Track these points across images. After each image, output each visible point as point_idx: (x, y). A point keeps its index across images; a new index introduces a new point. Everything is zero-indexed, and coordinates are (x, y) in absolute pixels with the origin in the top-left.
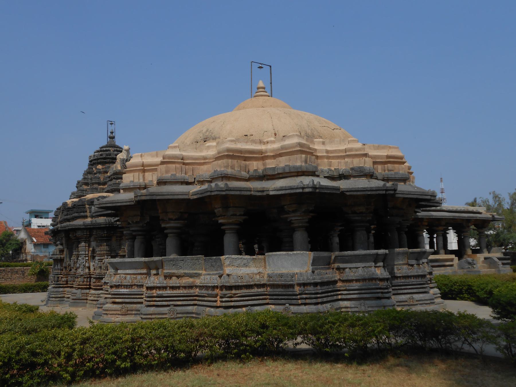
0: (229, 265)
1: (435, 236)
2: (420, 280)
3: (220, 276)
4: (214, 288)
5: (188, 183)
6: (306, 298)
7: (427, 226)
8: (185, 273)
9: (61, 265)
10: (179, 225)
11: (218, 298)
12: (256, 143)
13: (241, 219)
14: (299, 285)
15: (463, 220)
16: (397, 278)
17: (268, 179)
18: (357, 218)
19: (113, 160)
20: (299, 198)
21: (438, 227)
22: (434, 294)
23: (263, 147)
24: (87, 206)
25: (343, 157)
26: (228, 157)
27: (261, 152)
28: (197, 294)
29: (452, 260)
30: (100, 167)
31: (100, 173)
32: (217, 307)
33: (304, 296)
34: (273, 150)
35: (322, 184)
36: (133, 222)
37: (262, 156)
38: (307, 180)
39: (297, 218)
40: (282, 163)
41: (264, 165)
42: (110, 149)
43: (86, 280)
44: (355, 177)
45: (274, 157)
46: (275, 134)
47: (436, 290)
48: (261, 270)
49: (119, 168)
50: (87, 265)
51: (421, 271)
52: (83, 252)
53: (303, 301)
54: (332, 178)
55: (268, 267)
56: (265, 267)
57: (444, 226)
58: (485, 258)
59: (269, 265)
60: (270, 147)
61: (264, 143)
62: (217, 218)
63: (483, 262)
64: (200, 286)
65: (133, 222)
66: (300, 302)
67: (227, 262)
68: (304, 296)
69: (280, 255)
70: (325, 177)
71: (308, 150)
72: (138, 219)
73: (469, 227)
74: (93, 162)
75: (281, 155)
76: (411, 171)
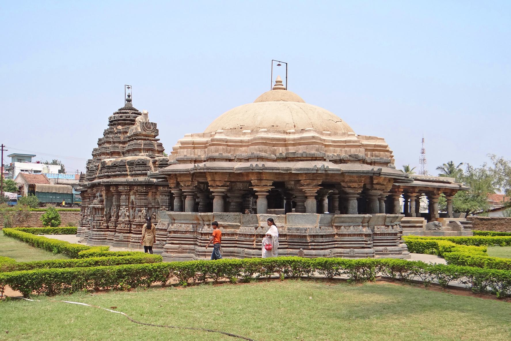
0: (262, 220)
1: (409, 200)
2: (393, 237)
3: (256, 228)
4: (251, 235)
5: (230, 160)
6: (315, 245)
7: (403, 192)
8: (229, 225)
9: (102, 214)
10: (223, 190)
11: (254, 243)
12: (281, 133)
13: (269, 188)
14: (311, 236)
15: (434, 188)
16: (376, 234)
17: (289, 161)
18: (351, 191)
19: (132, 122)
20: (312, 175)
21: (411, 192)
22: (402, 248)
23: (286, 137)
24: (127, 166)
25: (344, 147)
26: (263, 144)
27: (285, 140)
28: (237, 239)
29: (422, 222)
30: (120, 127)
31: (120, 133)
32: (254, 249)
33: (314, 244)
34: (294, 140)
35: (330, 167)
36: (185, 185)
37: (285, 143)
38: (319, 164)
39: (311, 190)
40: (301, 150)
41: (287, 150)
42: (129, 111)
43: (127, 226)
44: (351, 161)
45: (294, 145)
46: (295, 126)
47: (404, 245)
48: (283, 224)
49: (140, 130)
50: (127, 214)
51: (393, 230)
52: (124, 204)
53: (313, 247)
54: (335, 162)
55: (288, 223)
56: (286, 223)
57: (417, 193)
58: (450, 222)
59: (289, 222)
60: (291, 137)
61: (287, 133)
62: (252, 187)
63: (448, 225)
64: (240, 234)
65: (185, 185)
66: (310, 247)
67: (261, 219)
68: (314, 244)
69: (297, 215)
70: (330, 161)
71: (320, 142)
72: (190, 183)
73: (439, 194)
74: (113, 123)
75: (300, 144)
76: (392, 154)
